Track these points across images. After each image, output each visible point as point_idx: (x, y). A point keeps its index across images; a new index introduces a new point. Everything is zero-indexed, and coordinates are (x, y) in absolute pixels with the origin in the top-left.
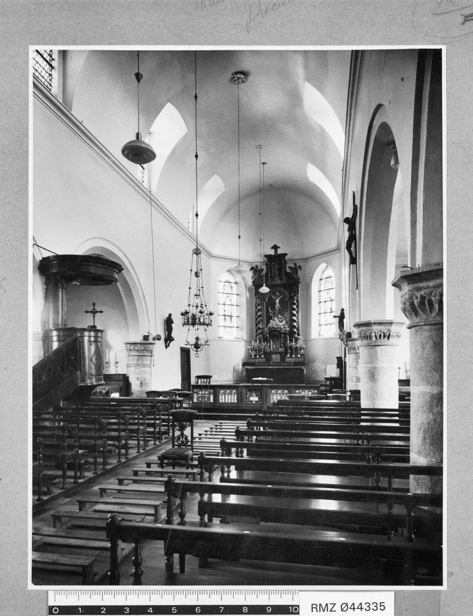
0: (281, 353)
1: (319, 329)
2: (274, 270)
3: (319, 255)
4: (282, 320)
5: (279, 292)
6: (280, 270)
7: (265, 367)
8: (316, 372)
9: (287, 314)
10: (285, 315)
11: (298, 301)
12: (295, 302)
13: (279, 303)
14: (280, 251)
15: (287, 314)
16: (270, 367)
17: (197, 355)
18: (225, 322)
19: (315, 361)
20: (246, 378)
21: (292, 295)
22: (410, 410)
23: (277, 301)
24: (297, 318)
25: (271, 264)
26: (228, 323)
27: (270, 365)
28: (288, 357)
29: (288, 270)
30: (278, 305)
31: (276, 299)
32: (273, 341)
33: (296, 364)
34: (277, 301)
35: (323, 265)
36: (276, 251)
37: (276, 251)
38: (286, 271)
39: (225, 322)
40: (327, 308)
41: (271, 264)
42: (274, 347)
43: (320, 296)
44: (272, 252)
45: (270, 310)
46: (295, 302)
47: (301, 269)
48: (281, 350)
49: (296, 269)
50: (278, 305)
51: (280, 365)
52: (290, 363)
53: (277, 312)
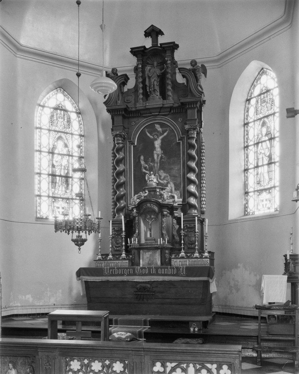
0: (162, 249)
1: (244, 202)
2: (149, 78)
3: (252, 40)
4: (168, 183)
5: (162, 125)
6: (162, 78)
7: (125, 278)
8: (238, 290)
9: (177, 169)
10: (174, 172)
11: (199, 141)
12: (194, 142)
13: (162, 148)
14: (161, 40)
15: (177, 169)
16: (137, 279)
17: (80, 252)
18: (54, 187)
19: (237, 267)
20: (85, 301)
21: (187, 127)
22: (287, 279)
23: (158, 144)
24: (196, 165)
25: (143, 67)
26: (60, 191)
27: (134, 274)
28: (110, 260)
29: (180, 79)
30: (158, 150)
31: (156, 140)
32: (146, 224)
33: (191, 271)
34: (158, 144)
35: (254, 66)
36: (155, 41)
37: (155, 41)
38: (174, 82)
39: (54, 187)
40: (260, 156)
41: (143, 67)
42: (148, 236)
43: (246, 133)
44: (148, 43)
45: (142, 163)
46: (194, 142)
47: (205, 73)
48: (160, 241)
49: (195, 71)
50: (158, 150)
51: (157, 274)
52: (178, 268)
53: (157, 166)
